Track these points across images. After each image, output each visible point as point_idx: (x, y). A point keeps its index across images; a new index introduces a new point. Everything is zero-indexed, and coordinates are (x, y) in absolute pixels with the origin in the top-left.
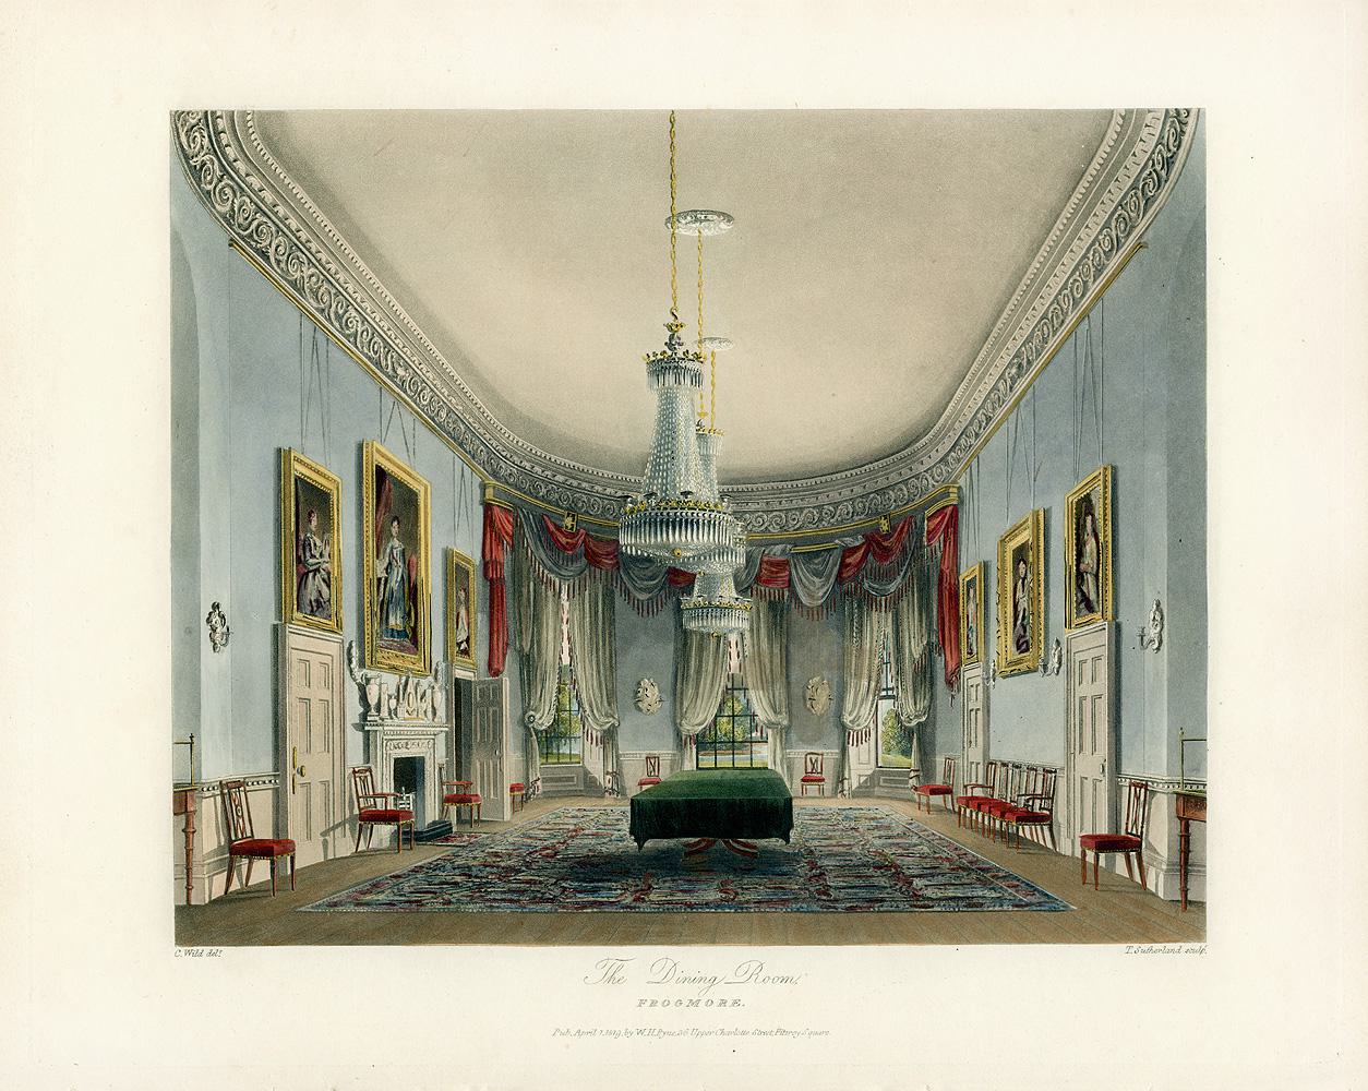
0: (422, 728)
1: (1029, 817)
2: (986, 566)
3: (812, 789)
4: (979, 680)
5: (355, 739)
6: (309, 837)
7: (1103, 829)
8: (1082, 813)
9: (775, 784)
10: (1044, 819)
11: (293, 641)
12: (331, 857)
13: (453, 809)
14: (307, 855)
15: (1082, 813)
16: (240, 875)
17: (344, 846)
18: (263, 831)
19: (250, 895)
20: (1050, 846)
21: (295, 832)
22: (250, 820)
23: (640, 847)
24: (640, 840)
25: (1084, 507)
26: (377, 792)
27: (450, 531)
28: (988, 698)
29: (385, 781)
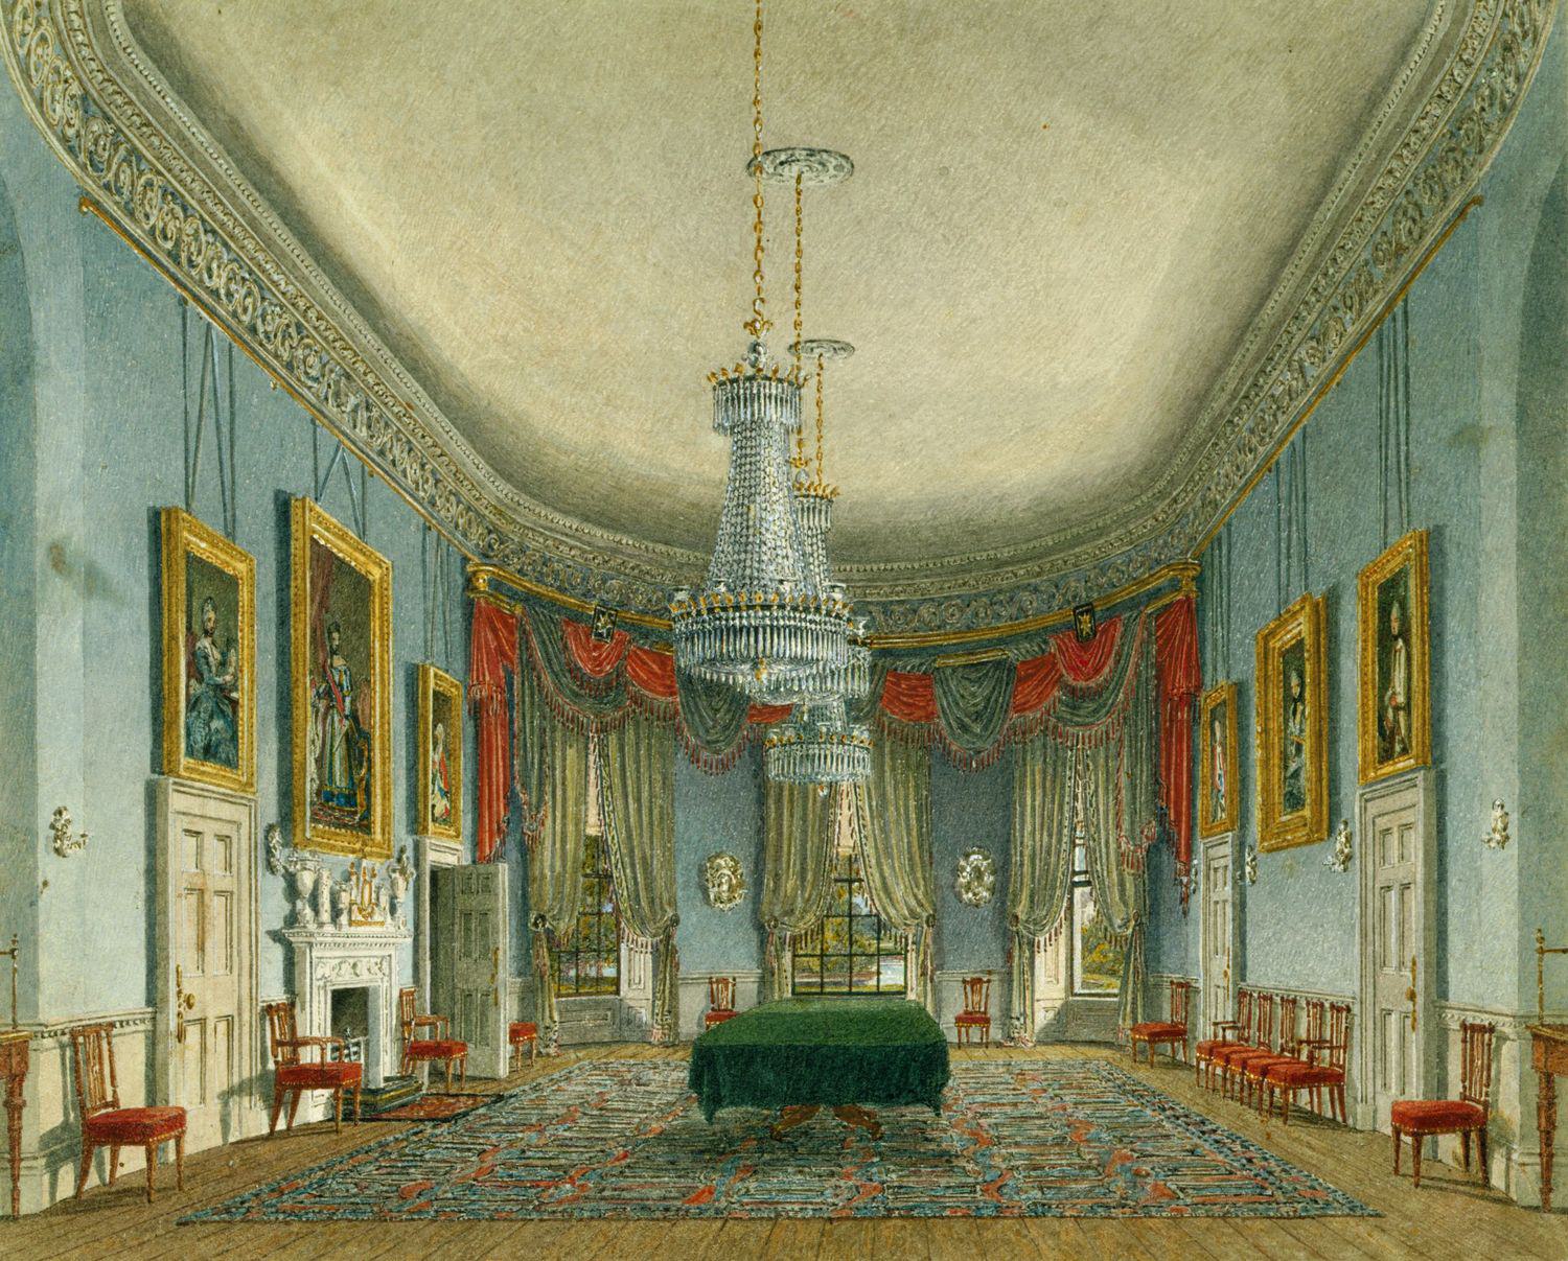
0: (377, 952)
1: (1312, 1078)
2: (1240, 689)
3: (975, 1034)
4: (1229, 861)
5: (273, 958)
6: (203, 1099)
7: (1416, 1093)
8: (1387, 1078)
9: (918, 1020)
10: (1335, 1078)
11: (176, 802)
12: (232, 1139)
13: (425, 1067)
14: (202, 1135)
15: (1387, 1078)
16: (100, 1165)
17: (254, 1119)
18: (131, 1095)
19: (118, 1196)
20: (1339, 1119)
21: (182, 1093)
22: (113, 1077)
23: (710, 1118)
24: (712, 1103)
25: (1390, 592)
26: (300, 1034)
27: (410, 635)
28: (1243, 942)
29: (316, 1018)
